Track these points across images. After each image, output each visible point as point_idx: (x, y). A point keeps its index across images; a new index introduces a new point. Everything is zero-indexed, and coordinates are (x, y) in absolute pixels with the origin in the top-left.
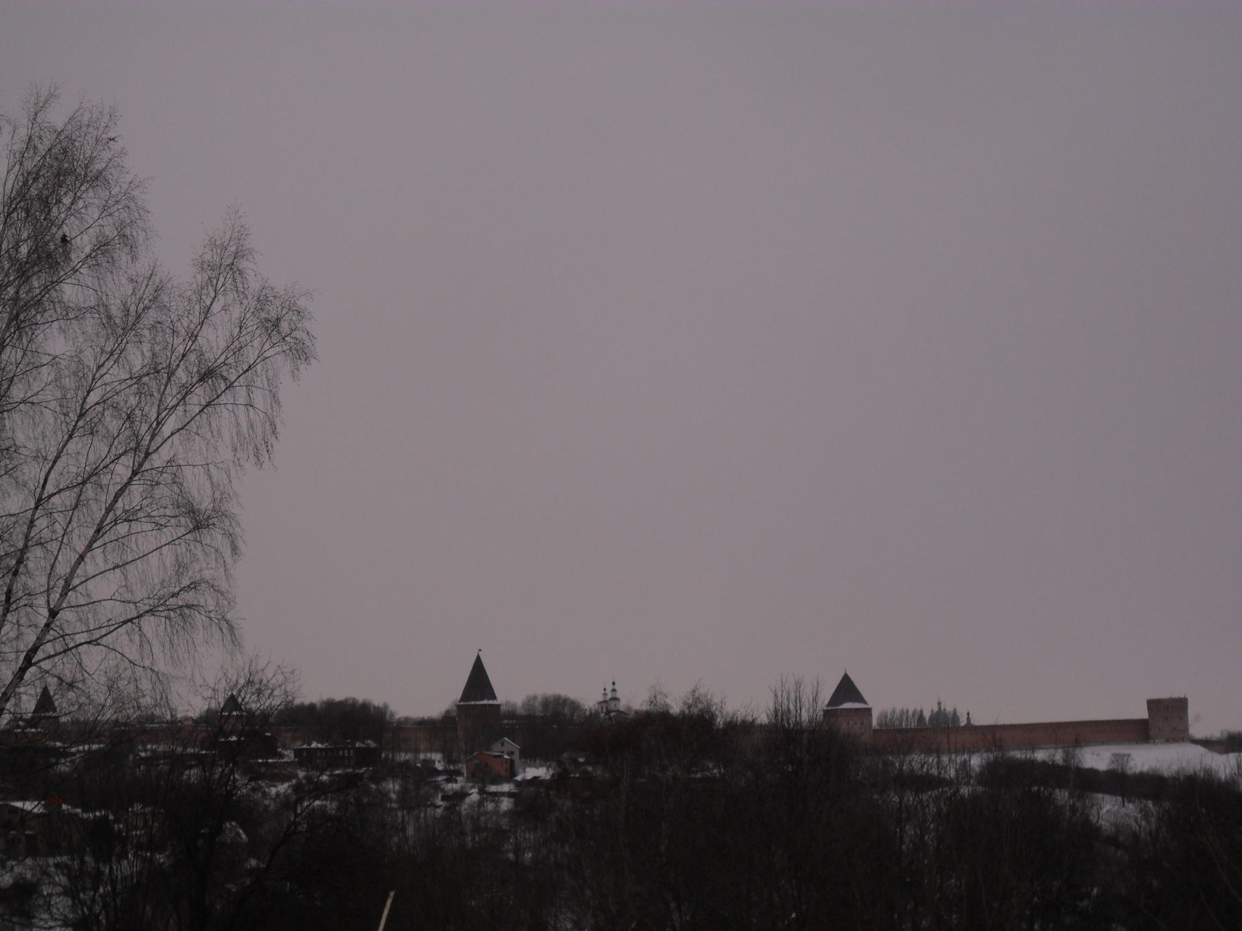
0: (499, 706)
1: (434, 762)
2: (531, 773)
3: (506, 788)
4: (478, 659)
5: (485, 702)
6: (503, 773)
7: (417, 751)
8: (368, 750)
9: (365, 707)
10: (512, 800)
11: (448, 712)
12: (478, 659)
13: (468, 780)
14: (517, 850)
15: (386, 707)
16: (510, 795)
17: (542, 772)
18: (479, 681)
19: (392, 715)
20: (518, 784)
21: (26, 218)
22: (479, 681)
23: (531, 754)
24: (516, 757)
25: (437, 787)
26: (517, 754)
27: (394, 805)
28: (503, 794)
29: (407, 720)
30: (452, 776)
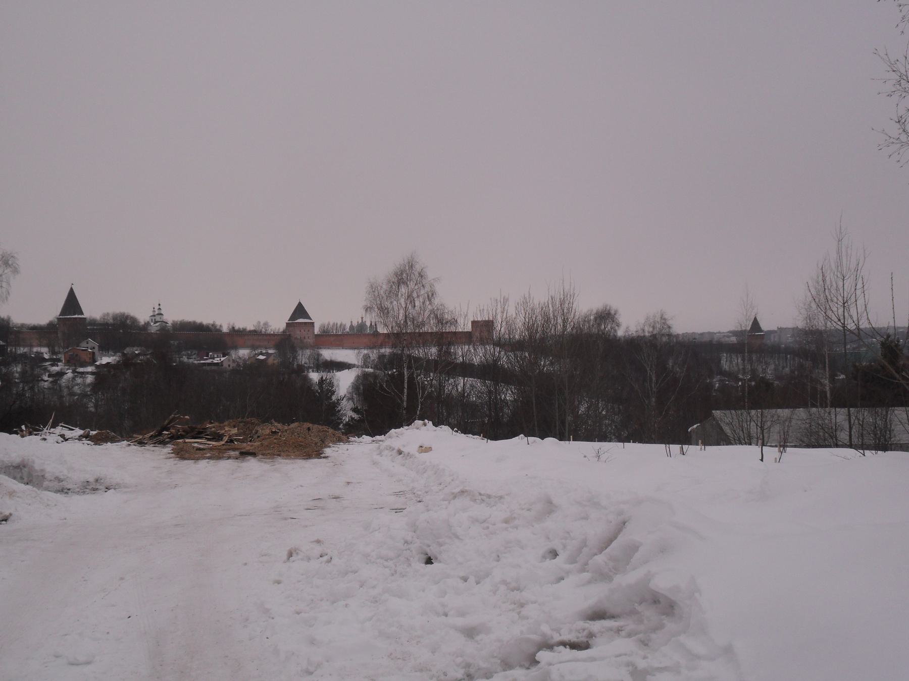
2: (105, 360)
3: (90, 369)
4: (755, 319)
5: (76, 316)
6: (88, 360)
7: (31, 346)
12: (755, 319)
15: (9, 318)
16: (92, 373)
18: (72, 303)
20: (97, 367)
22: (72, 303)
23: (105, 348)
24: (96, 350)
25: (46, 370)
26: (97, 348)
28: (88, 373)
29: (23, 325)
30: (55, 362)
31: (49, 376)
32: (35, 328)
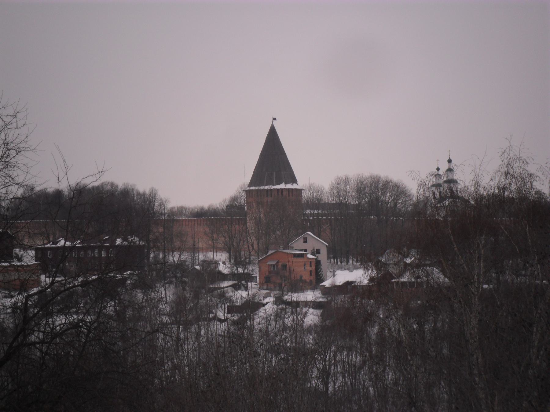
0: (299, 191)
1: (217, 263)
2: (342, 277)
3: (309, 296)
4: (272, 138)
5: (282, 186)
6: (306, 277)
7: (195, 250)
8: (130, 250)
9: (126, 193)
10: (318, 312)
11: (234, 199)
12: (272, 138)
13: (261, 286)
14: (325, 375)
15: (153, 194)
16: (316, 305)
17: (359, 276)
18: (273, 159)
19: (162, 204)
20: (326, 291)
21: (369, 320)
22: (273, 159)
23: (340, 253)
24: (323, 257)
25: (222, 296)
26: (324, 252)
27: (165, 319)
28: (307, 304)
29: (181, 210)
30: (241, 281)
31: (230, 310)
32: (204, 216)
